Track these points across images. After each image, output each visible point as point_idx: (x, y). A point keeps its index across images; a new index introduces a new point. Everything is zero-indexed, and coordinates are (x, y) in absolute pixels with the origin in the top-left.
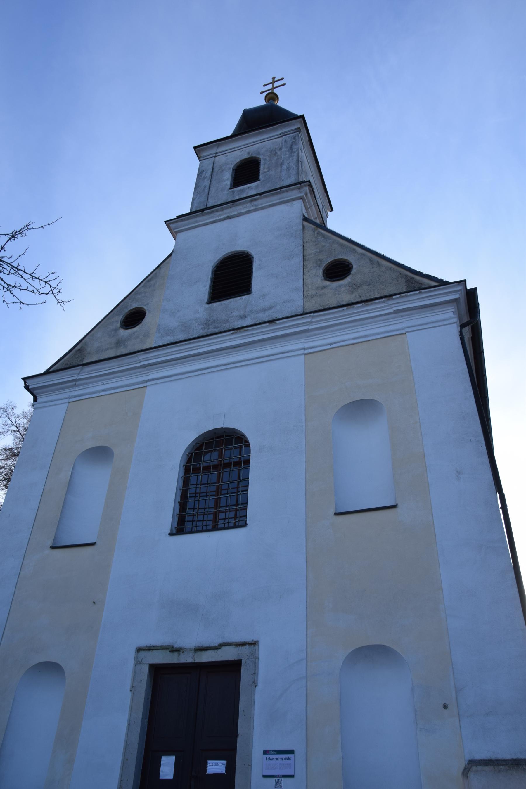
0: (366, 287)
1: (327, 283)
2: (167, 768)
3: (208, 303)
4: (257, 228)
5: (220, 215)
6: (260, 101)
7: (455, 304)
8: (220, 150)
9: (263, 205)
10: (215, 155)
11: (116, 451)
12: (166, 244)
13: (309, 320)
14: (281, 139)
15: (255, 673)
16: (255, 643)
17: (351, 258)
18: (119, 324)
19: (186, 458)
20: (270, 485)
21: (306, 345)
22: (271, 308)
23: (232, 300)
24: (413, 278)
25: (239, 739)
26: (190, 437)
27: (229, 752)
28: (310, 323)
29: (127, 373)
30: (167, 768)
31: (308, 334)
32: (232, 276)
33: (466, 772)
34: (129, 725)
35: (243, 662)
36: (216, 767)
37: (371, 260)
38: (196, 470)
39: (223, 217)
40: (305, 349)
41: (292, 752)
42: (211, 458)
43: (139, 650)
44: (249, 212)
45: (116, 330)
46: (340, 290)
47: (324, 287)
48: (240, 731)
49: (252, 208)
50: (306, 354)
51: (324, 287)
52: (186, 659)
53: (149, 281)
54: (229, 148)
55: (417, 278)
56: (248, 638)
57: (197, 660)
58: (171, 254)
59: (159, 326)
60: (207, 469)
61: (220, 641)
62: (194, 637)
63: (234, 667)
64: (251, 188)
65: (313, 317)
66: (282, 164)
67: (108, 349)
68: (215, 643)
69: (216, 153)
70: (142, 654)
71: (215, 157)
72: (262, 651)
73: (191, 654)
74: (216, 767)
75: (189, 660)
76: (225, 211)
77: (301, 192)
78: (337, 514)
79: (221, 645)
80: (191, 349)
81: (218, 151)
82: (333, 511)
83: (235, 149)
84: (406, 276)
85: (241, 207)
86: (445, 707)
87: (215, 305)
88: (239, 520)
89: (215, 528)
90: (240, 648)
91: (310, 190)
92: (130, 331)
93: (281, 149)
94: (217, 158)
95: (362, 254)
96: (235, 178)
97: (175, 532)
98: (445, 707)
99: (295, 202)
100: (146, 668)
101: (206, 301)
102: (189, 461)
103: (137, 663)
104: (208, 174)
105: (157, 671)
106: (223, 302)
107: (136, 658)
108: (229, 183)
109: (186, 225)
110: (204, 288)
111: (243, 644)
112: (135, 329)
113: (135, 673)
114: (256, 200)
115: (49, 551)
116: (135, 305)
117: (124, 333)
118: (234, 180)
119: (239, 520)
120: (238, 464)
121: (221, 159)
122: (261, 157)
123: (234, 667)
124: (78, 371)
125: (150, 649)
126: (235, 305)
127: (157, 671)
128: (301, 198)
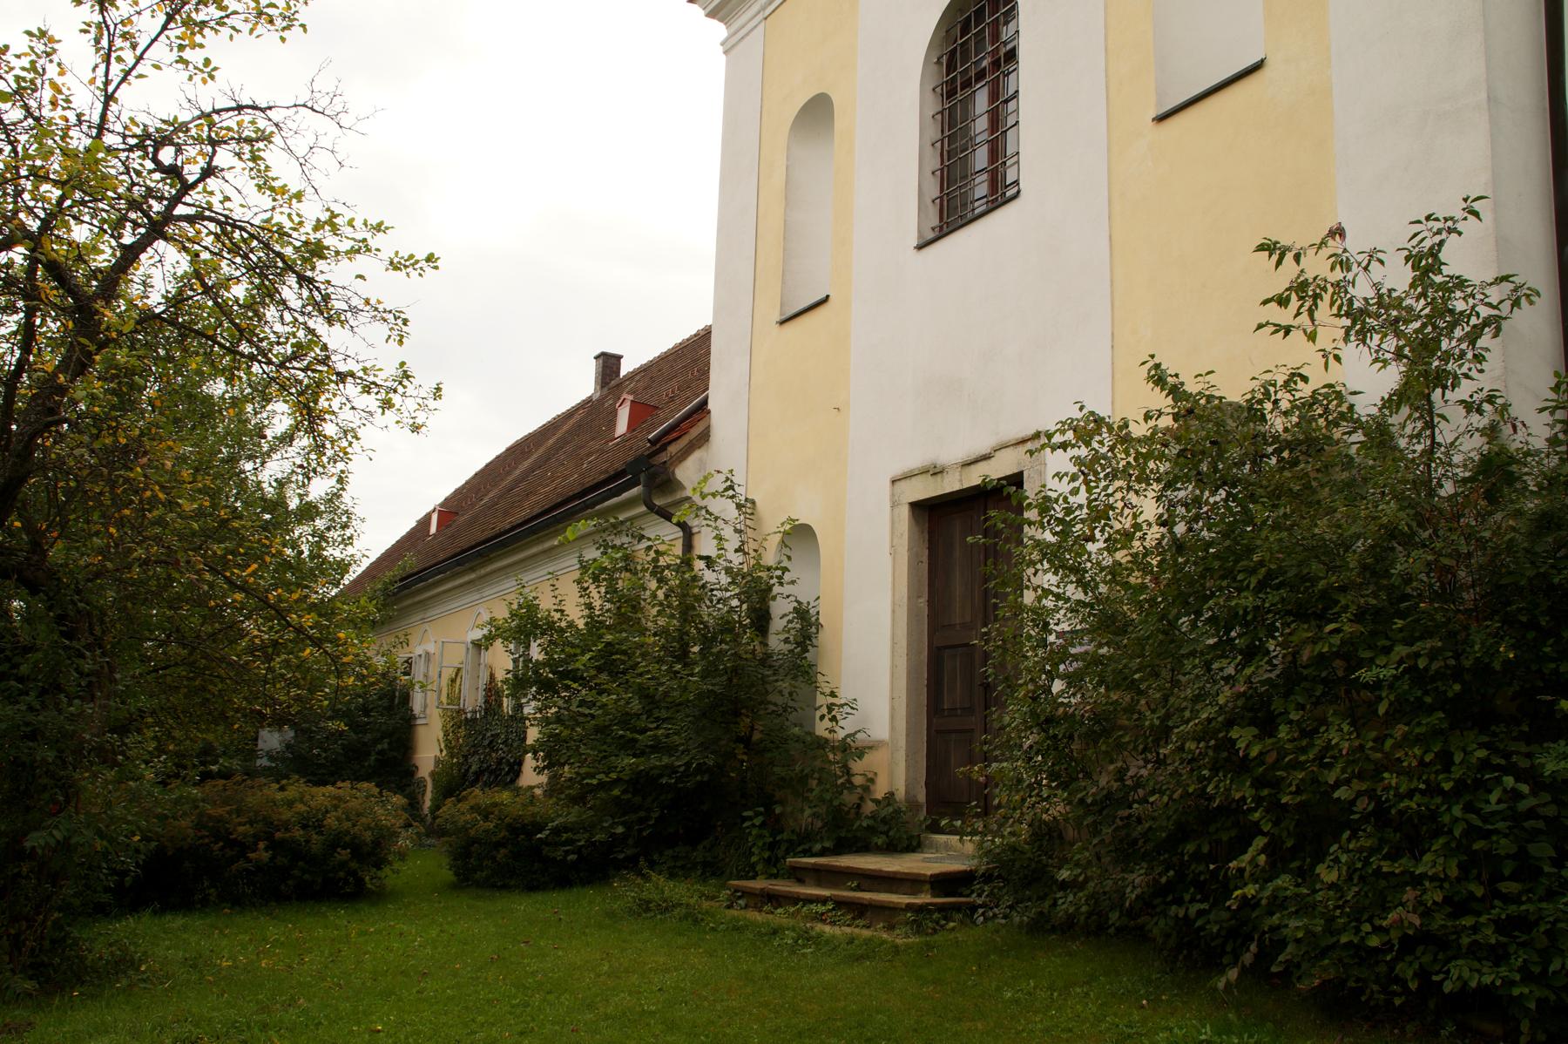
78: (1161, 118)
103: (894, 505)
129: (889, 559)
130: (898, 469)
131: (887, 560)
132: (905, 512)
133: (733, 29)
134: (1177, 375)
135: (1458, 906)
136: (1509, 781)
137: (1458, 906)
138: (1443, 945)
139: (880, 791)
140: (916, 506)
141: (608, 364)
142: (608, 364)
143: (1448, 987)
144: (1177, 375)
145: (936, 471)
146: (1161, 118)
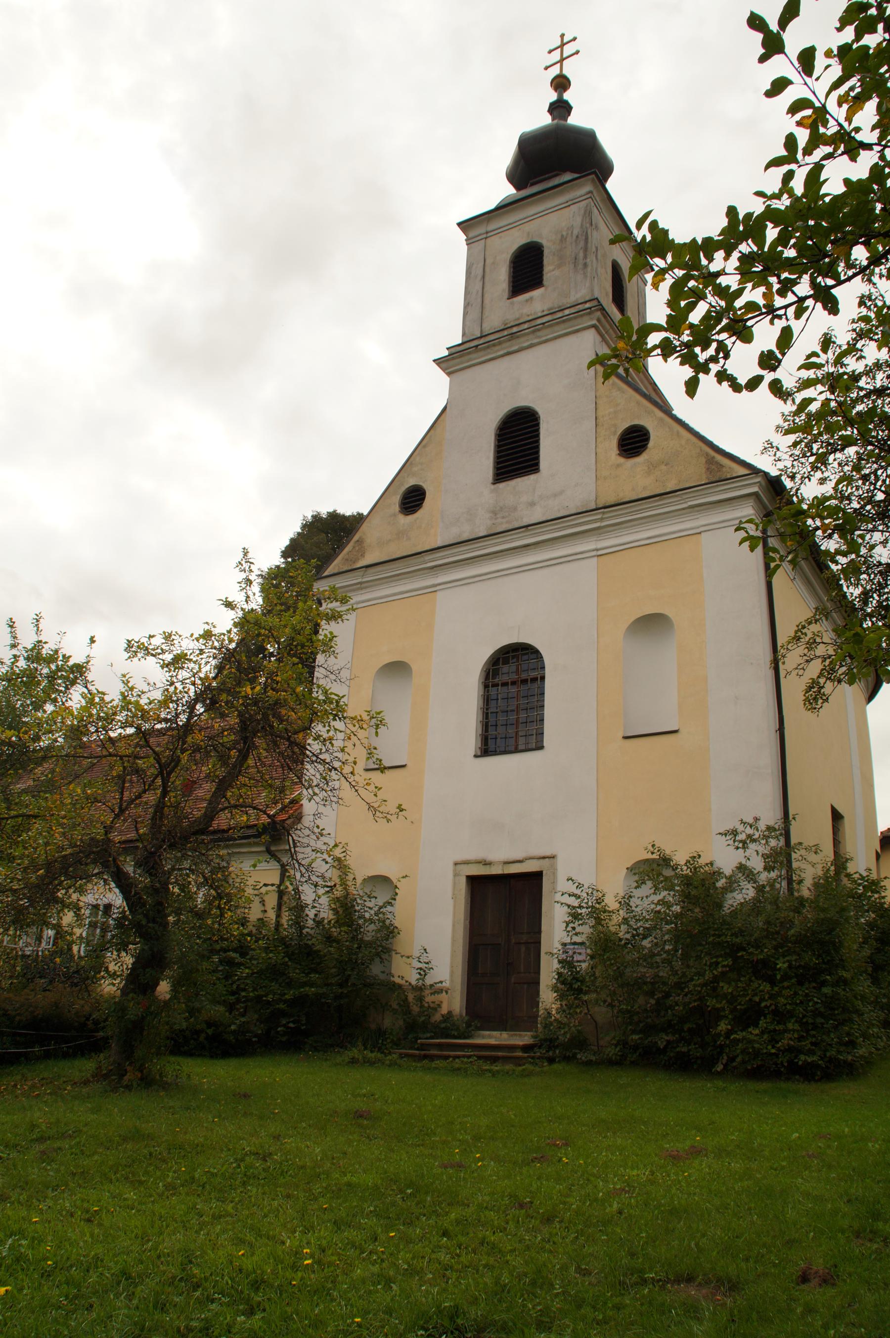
0: (663, 467)
1: (622, 460)
3: (494, 484)
5: (499, 350)
6: (545, 120)
7: (754, 497)
9: (549, 337)
10: (485, 236)
11: (414, 667)
12: (446, 353)
13: (599, 517)
16: (553, 857)
18: (397, 508)
19: (484, 674)
21: (599, 546)
22: (562, 492)
23: (519, 480)
24: (713, 457)
25: (543, 935)
28: (602, 519)
29: (415, 574)
31: (602, 531)
32: (518, 444)
34: (454, 925)
35: (544, 873)
38: (495, 685)
39: (501, 353)
40: (597, 550)
42: (507, 672)
43: (456, 864)
44: (531, 346)
45: (395, 515)
46: (636, 476)
48: (543, 928)
49: (535, 341)
50: (598, 556)
52: (496, 870)
53: (425, 447)
54: (501, 224)
55: (719, 458)
56: (548, 854)
57: (506, 872)
58: (444, 409)
60: (505, 684)
62: (503, 853)
63: (536, 878)
64: (536, 302)
65: (604, 513)
69: (487, 233)
70: (459, 867)
71: (486, 238)
72: (560, 863)
73: (500, 867)
75: (500, 872)
76: (504, 345)
77: (592, 319)
78: (626, 738)
80: (479, 549)
81: (489, 229)
82: (621, 735)
83: (510, 227)
84: (707, 454)
85: (521, 340)
89: (516, 750)
90: (541, 861)
91: (602, 314)
92: (411, 518)
94: (489, 240)
95: (661, 420)
96: (514, 277)
97: (479, 754)
100: (464, 880)
102: (487, 677)
103: (456, 875)
105: (474, 881)
107: (455, 870)
109: (459, 364)
111: (544, 858)
113: (454, 884)
114: (539, 330)
116: (412, 482)
117: (404, 520)
118: (513, 282)
120: (534, 680)
121: (495, 242)
123: (536, 878)
124: (361, 573)
125: (467, 863)
127: (474, 881)
128: (594, 326)
129: (451, 902)
130: (459, 857)
131: (450, 903)
132: (463, 881)
133: (524, 193)
134: (712, 864)
135: (800, 1038)
136: (815, 999)
137: (800, 1038)
138: (798, 1051)
139: (444, 1010)
140: (468, 877)
141: (732, 212)
142: (732, 212)
143: (800, 1063)
144: (712, 864)
145: (486, 863)
146: (626, 738)
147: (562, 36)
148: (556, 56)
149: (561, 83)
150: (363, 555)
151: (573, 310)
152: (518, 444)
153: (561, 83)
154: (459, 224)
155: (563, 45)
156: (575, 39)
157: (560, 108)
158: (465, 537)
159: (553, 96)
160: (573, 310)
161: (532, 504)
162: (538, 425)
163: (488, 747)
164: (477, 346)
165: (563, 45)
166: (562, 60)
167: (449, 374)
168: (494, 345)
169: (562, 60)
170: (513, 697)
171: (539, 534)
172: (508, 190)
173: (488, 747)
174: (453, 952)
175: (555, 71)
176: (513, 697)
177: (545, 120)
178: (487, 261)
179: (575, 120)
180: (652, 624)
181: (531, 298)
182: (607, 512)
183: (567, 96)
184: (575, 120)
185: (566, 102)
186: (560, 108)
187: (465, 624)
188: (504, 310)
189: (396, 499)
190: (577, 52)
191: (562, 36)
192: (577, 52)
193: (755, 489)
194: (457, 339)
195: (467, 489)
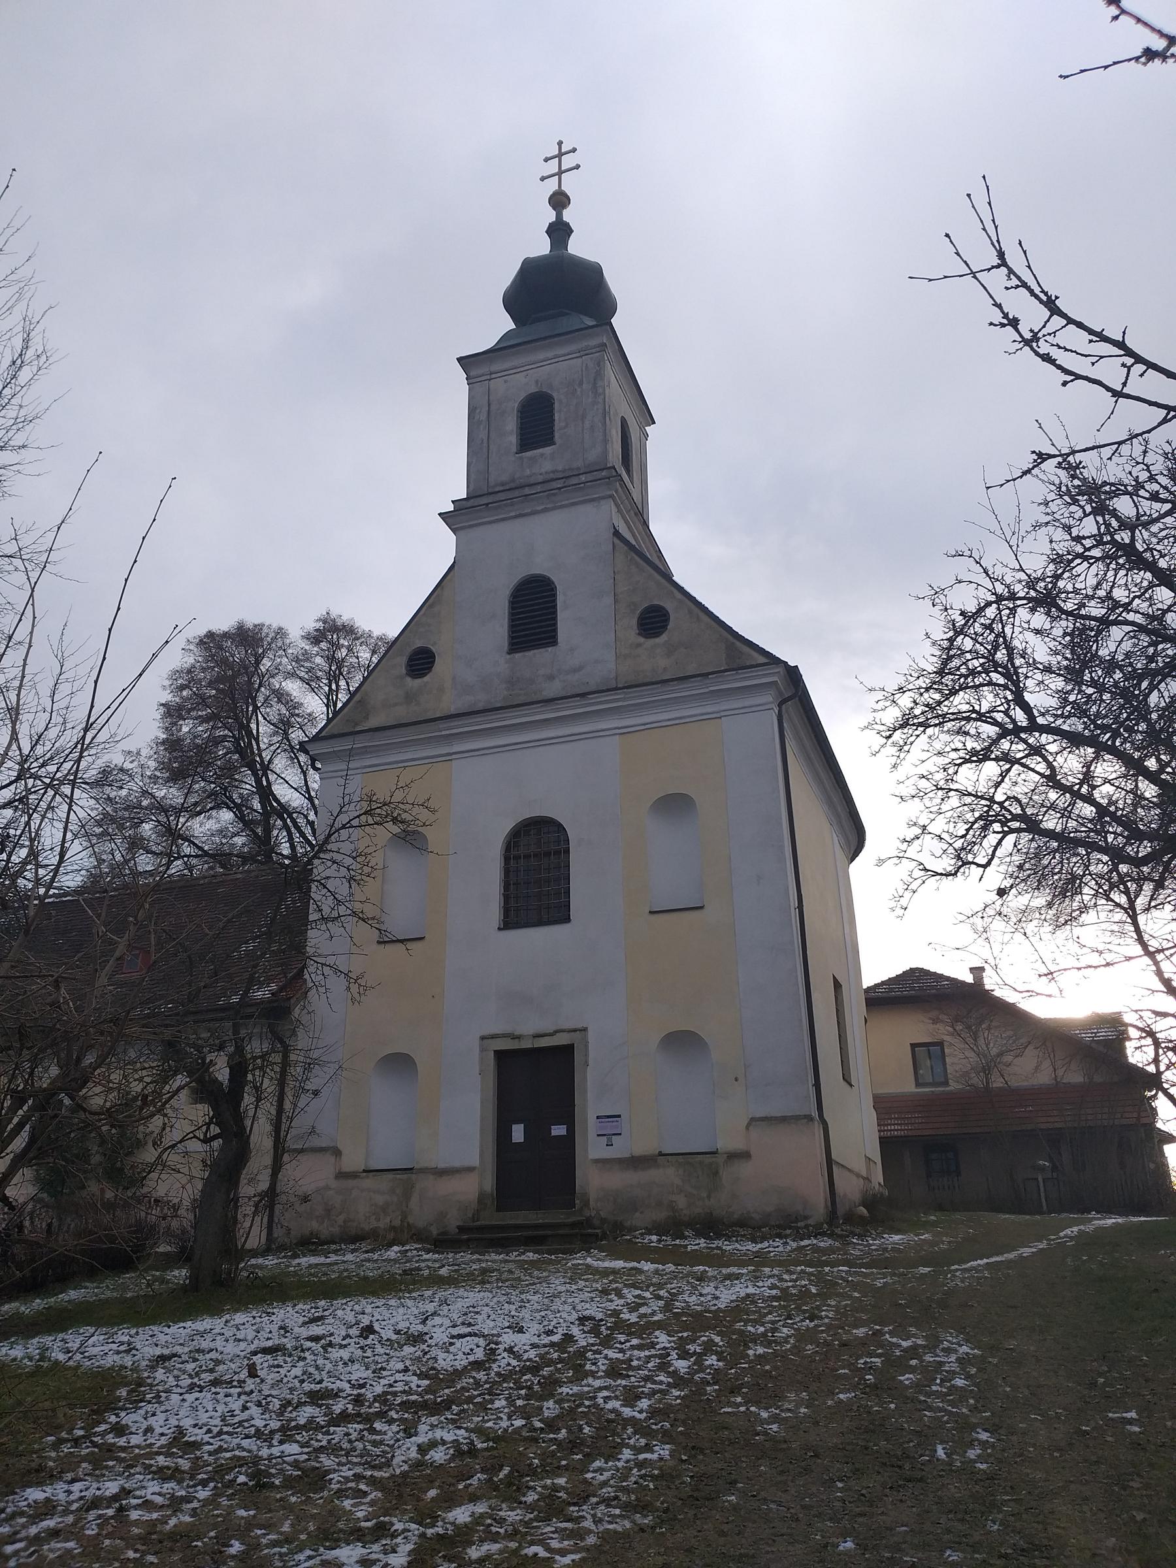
1: (642, 640)
2: (518, 1133)
4: (556, 541)
6: (542, 247)
8: (495, 368)
12: (451, 508)
14: (580, 360)
15: (587, 1055)
16: (585, 1030)
17: (668, 605)
18: (404, 671)
20: (479, 882)
22: (581, 668)
26: (508, 825)
27: (568, 1116)
30: (518, 1133)
32: (533, 613)
33: (747, 1127)
36: (558, 1130)
37: (690, 612)
39: (513, 514)
41: (619, 1116)
43: (483, 1038)
44: (546, 510)
46: (654, 656)
47: (639, 645)
51: (639, 645)
52: (526, 1044)
53: (431, 606)
55: (738, 644)
56: (579, 1026)
59: (454, 678)
60: (527, 857)
61: (555, 1028)
62: (531, 1025)
63: (567, 1051)
64: (546, 461)
66: (583, 417)
67: (396, 705)
68: (551, 1029)
74: (558, 1130)
79: (556, 1032)
86: (736, 1080)
87: (517, 656)
88: (564, 917)
92: (418, 681)
93: (581, 383)
98: (736, 1080)
99: (602, 502)
101: (506, 648)
103: (483, 1050)
104: (483, 417)
105: (501, 1056)
106: (527, 654)
107: (481, 1046)
108: (513, 440)
110: (500, 629)
111: (575, 1030)
112: (426, 679)
114: (554, 495)
115: (375, 946)
116: (419, 643)
117: (413, 684)
119: (564, 917)
121: (498, 385)
122: (555, 395)
123: (567, 1051)
125: (493, 1037)
126: (540, 657)
127: (501, 1056)
147: (560, 143)
148: (553, 167)
149: (559, 201)
150: (367, 718)
151: (590, 477)
152: (533, 613)
153: (559, 201)
154: (459, 360)
155: (560, 155)
156: (574, 150)
157: (559, 232)
158: (480, 706)
159: (551, 216)
160: (590, 477)
161: (551, 678)
162: (555, 595)
163: (512, 919)
164: (487, 504)
165: (560, 155)
166: (560, 173)
167: (454, 531)
168: (506, 505)
169: (560, 173)
170: (536, 870)
171: (558, 710)
172: (507, 324)
173: (512, 919)
174: (482, 1119)
175: (552, 186)
176: (536, 870)
177: (542, 247)
178: (492, 408)
179: (576, 247)
180: (675, 805)
181: (542, 455)
182: (626, 689)
183: (567, 215)
184: (576, 247)
185: (567, 225)
186: (559, 232)
187: (481, 795)
188: (508, 464)
189: (402, 661)
190: (578, 167)
191: (560, 143)
192: (578, 167)
193: (775, 679)
194: (461, 492)
195: (479, 648)
